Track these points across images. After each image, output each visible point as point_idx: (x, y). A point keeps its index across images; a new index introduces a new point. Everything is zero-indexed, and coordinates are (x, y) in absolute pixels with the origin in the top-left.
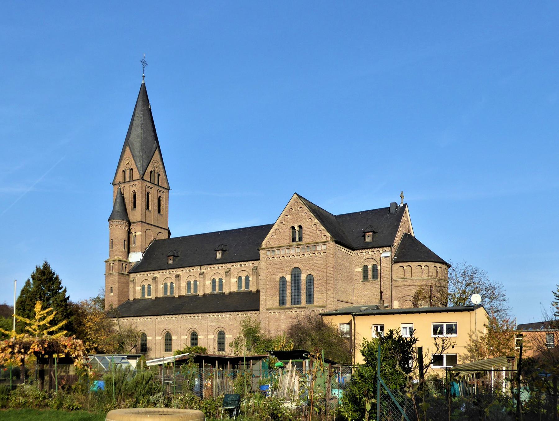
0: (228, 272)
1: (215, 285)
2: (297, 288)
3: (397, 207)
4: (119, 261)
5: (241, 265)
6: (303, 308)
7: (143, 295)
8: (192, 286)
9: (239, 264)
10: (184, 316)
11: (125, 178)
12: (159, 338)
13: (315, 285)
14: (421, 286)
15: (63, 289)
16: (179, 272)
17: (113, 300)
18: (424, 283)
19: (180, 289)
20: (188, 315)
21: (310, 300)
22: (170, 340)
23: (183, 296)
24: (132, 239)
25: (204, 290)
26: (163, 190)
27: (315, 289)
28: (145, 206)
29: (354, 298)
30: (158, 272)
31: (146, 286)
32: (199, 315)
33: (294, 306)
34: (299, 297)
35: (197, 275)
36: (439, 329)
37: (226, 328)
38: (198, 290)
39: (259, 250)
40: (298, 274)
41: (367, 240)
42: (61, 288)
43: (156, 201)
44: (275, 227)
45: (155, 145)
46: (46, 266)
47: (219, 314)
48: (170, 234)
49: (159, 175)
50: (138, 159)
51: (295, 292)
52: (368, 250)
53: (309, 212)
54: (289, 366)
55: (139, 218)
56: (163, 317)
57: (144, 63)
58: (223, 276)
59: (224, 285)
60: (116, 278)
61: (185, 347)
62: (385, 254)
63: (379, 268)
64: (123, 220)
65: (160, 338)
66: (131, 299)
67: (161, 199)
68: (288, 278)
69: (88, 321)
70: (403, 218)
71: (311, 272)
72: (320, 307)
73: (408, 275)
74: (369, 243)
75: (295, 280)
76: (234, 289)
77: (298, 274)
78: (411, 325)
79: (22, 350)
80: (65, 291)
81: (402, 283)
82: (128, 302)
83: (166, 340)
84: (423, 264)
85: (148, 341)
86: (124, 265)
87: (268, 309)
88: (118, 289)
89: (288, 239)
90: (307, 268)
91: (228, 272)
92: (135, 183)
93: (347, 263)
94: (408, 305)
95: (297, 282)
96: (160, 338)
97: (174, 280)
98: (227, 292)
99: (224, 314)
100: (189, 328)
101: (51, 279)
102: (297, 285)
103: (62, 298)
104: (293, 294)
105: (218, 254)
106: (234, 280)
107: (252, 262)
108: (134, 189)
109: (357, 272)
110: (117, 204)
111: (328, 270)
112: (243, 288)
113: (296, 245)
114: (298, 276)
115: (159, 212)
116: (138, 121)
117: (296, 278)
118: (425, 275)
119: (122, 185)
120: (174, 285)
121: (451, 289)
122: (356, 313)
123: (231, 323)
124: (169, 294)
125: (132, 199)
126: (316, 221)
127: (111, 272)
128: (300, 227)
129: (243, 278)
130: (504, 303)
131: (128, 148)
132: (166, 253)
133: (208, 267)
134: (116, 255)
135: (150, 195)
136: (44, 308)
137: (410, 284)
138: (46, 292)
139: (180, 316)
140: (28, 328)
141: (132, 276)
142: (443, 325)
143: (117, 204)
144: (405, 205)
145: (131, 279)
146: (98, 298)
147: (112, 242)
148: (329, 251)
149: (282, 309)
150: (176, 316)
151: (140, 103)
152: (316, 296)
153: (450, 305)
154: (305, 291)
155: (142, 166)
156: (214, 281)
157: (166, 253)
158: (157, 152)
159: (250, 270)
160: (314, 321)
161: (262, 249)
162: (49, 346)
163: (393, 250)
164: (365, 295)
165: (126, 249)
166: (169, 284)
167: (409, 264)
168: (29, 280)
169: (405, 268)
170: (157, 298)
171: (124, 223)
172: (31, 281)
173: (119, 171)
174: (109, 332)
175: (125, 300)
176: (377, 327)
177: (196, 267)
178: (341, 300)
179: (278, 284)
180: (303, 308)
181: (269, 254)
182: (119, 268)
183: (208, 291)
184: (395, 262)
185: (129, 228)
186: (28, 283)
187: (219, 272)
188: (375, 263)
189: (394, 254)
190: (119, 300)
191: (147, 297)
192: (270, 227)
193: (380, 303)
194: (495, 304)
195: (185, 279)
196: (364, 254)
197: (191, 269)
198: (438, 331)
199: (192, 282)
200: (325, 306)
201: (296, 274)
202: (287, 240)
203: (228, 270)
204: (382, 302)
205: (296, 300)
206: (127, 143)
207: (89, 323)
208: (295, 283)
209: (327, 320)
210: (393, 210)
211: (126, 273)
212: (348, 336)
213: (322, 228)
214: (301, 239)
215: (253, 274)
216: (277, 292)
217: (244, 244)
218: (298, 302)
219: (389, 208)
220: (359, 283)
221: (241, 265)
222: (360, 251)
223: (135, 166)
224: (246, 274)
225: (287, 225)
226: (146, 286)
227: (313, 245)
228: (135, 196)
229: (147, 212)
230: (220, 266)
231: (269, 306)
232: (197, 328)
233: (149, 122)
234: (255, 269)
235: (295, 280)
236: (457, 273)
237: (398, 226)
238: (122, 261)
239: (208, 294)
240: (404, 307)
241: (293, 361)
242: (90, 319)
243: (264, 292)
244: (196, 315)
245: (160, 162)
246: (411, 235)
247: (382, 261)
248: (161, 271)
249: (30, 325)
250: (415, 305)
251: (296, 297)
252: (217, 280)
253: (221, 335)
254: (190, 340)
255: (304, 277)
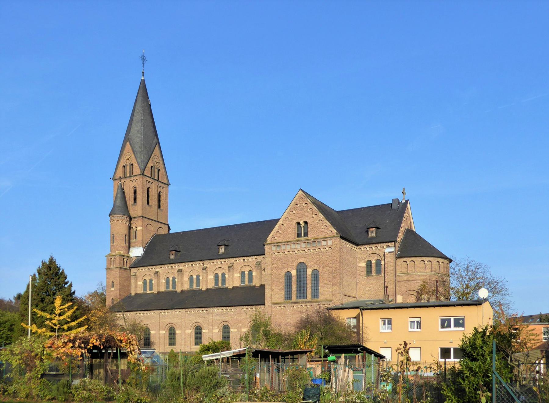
0: (231, 267)
1: (218, 280)
2: (302, 283)
3: (399, 203)
4: (120, 255)
5: (244, 260)
6: (309, 302)
7: (145, 289)
8: (195, 281)
9: (242, 259)
10: (188, 310)
11: (125, 173)
12: (163, 332)
13: (321, 280)
14: (424, 281)
15: (69, 283)
16: (181, 266)
17: (113, 295)
18: (428, 278)
19: (182, 284)
20: (192, 310)
21: (316, 294)
22: (174, 334)
23: (186, 291)
24: (132, 234)
25: (206, 285)
26: (163, 185)
27: (321, 284)
28: (145, 201)
29: (358, 293)
30: (160, 266)
31: (148, 281)
32: (204, 309)
33: (300, 300)
34: (305, 291)
35: (200, 270)
36: (446, 322)
37: (231, 322)
38: (201, 284)
39: (264, 245)
40: (303, 269)
41: (370, 235)
42: (66, 283)
43: (157, 196)
44: (280, 222)
45: (155, 140)
46: (52, 261)
47: (224, 309)
48: (169, 229)
49: (159, 170)
50: (139, 155)
51: (300, 287)
52: (372, 246)
53: (314, 208)
54: (342, 360)
55: (140, 214)
56: (166, 311)
57: (144, 59)
58: (226, 271)
59: (227, 279)
60: (118, 272)
61: (210, 341)
62: (389, 249)
63: (383, 263)
64: (124, 215)
65: (164, 332)
66: (133, 293)
67: (161, 194)
68: (294, 273)
69: (92, 316)
70: (406, 214)
71: (317, 267)
72: (325, 301)
73: (412, 269)
74: (372, 238)
75: (300, 275)
76: (237, 283)
77: (303, 269)
78: (418, 319)
79: (83, 345)
80: (71, 285)
81: (405, 278)
82: (130, 296)
83: (170, 334)
84: (426, 259)
85: (151, 335)
86: (125, 260)
87: (274, 304)
88: (120, 284)
89: (293, 235)
90: (312, 263)
91: (231, 267)
92: (135, 178)
93: (351, 258)
94: (412, 300)
95: (302, 276)
96: (164, 332)
97: (176, 275)
98: (230, 287)
99: (229, 308)
100: (193, 322)
101: (57, 274)
102: (302, 279)
103: (68, 293)
104: (299, 289)
105: (220, 249)
106: (237, 275)
107: (256, 257)
108: (135, 184)
109: (361, 267)
110: (118, 200)
111: (333, 266)
112: (247, 283)
113: (302, 241)
114: (304, 271)
115: (159, 207)
116: (138, 117)
117: (302, 273)
118: (428, 270)
119: (123, 181)
120: (176, 280)
121: (454, 283)
122: (363, 308)
123: (235, 317)
124: (171, 288)
125: (132, 194)
126: (321, 217)
127: (112, 267)
128: (306, 223)
129: (247, 273)
130: (507, 297)
131: (128, 143)
132: (167, 248)
133: (211, 261)
134: (117, 250)
135: (150, 190)
136: (62, 304)
137: (414, 278)
138: (52, 287)
139: (184, 310)
140: (48, 322)
141: (133, 270)
142: (450, 319)
143: (118, 200)
144: (407, 201)
145: (132, 274)
146: (96, 292)
147: (113, 237)
148: (334, 246)
149: (287, 303)
150: (180, 310)
151: (140, 99)
152: (322, 290)
153: (454, 299)
154: (310, 286)
155: (143, 161)
156: (216, 276)
157: (167, 248)
158: (157, 147)
159: (253, 265)
160: (322, 315)
161: (267, 244)
162: (106, 341)
163: (397, 245)
164: (369, 289)
165: (127, 244)
166: (171, 279)
167: (413, 259)
168: (35, 275)
169: (408, 263)
170: (159, 293)
171: (125, 218)
172: (37, 276)
173: (119, 166)
174: (114, 326)
175: (126, 294)
176: (385, 321)
177: (199, 262)
178: (346, 294)
179: (284, 278)
180: (309, 302)
181: (274, 249)
182: (120, 263)
183: (211, 285)
184: (399, 258)
185: (130, 223)
186: (34, 278)
187: (222, 267)
188: (379, 258)
189: (397, 249)
190: (120, 295)
191: (148, 292)
192: (272, 223)
193: (385, 298)
194: (498, 298)
195: (187, 274)
196: (368, 249)
197: (194, 264)
198: (446, 325)
199: (195, 277)
200: (331, 301)
201: (301, 268)
202: (292, 234)
203: (231, 265)
204: (387, 296)
205: (302, 294)
206: (127, 138)
207: (94, 318)
208: (300, 278)
209: (335, 313)
210: (395, 206)
211: (127, 267)
212: (355, 330)
213: (328, 224)
214: (306, 234)
215: (257, 269)
216: (282, 286)
217: (249, 239)
218: (304, 296)
219: (391, 204)
220: (363, 278)
221: (244, 260)
222: (364, 246)
223: (135, 161)
224: (249, 269)
225: (292, 221)
226: (148, 281)
227: (319, 240)
228: (135, 191)
229: (147, 207)
230: (223, 260)
231: (274, 301)
232: (202, 322)
233: (150, 118)
234: (258, 264)
235: (300, 275)
236: (461, 268)
237: (400, 222)
238: (124, 256)
239: (211, 289)
240: (408, 301)
241: (346, 355)
242: (94, 313)
243: (270, 287)
244: (200, 310)
245: (160, 158)
246: (412, 230)
247: (386, 256)
248: (163, 266)
249: (51, 319)
250: (419, 299)
251: (302, 292)
252: (220, 275)
253: (226, 329)
254: (194, 334)
255: (309, 272)
